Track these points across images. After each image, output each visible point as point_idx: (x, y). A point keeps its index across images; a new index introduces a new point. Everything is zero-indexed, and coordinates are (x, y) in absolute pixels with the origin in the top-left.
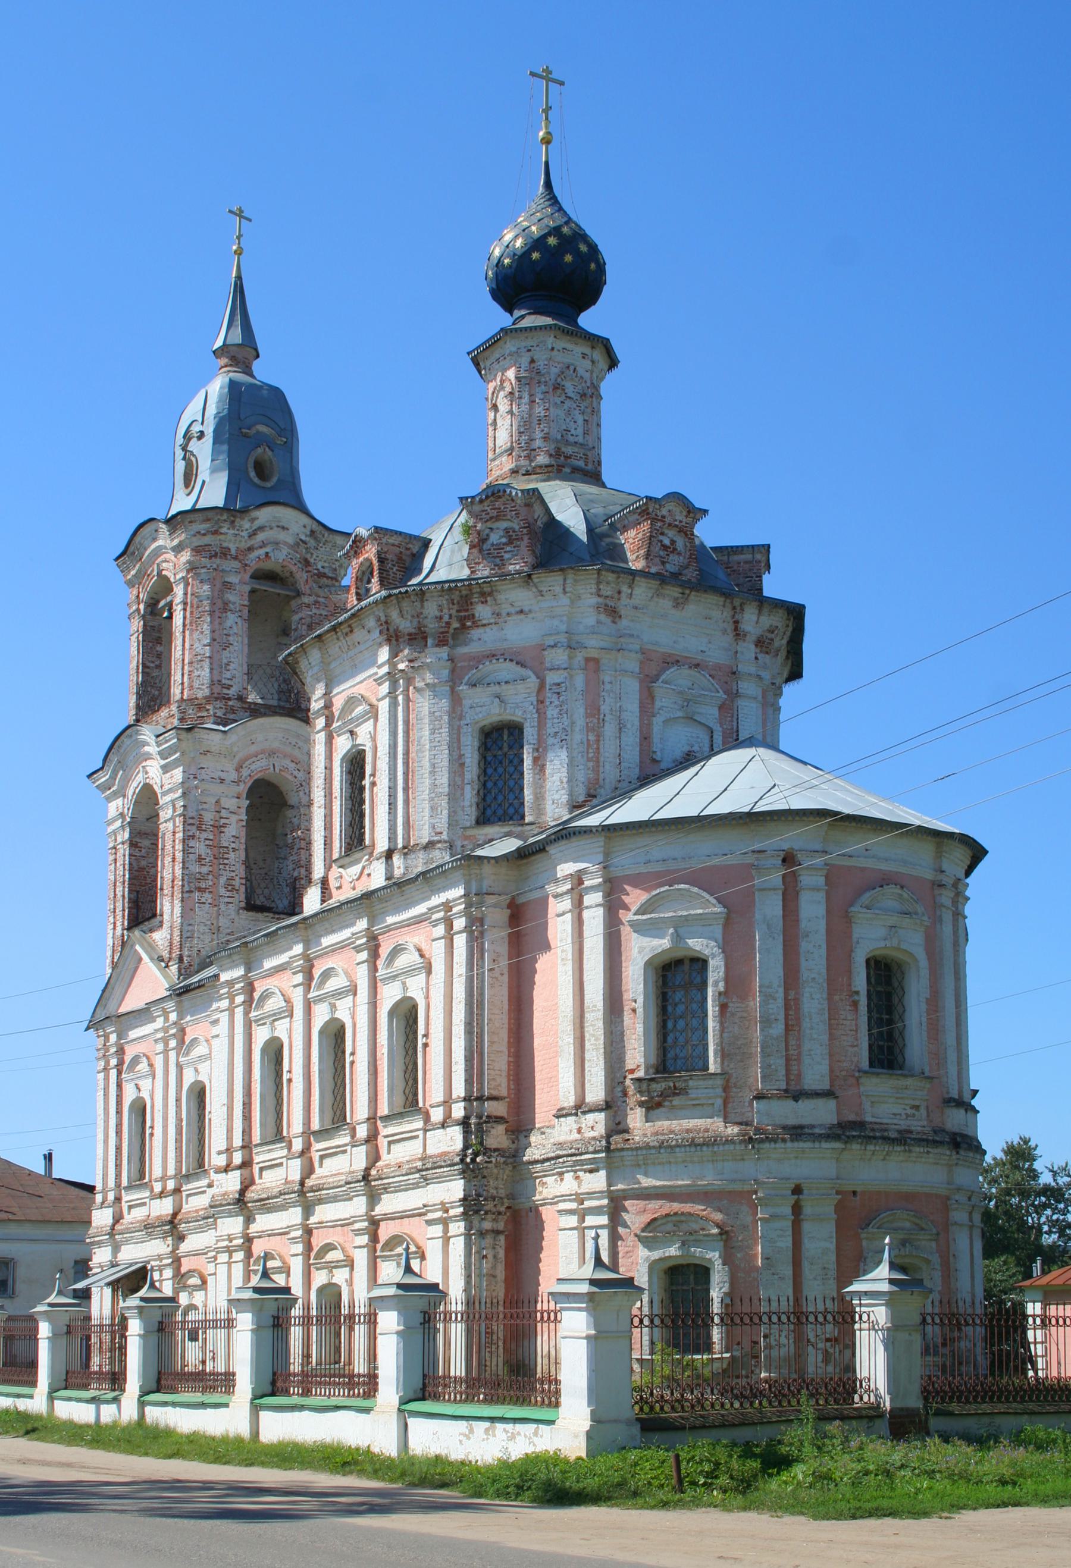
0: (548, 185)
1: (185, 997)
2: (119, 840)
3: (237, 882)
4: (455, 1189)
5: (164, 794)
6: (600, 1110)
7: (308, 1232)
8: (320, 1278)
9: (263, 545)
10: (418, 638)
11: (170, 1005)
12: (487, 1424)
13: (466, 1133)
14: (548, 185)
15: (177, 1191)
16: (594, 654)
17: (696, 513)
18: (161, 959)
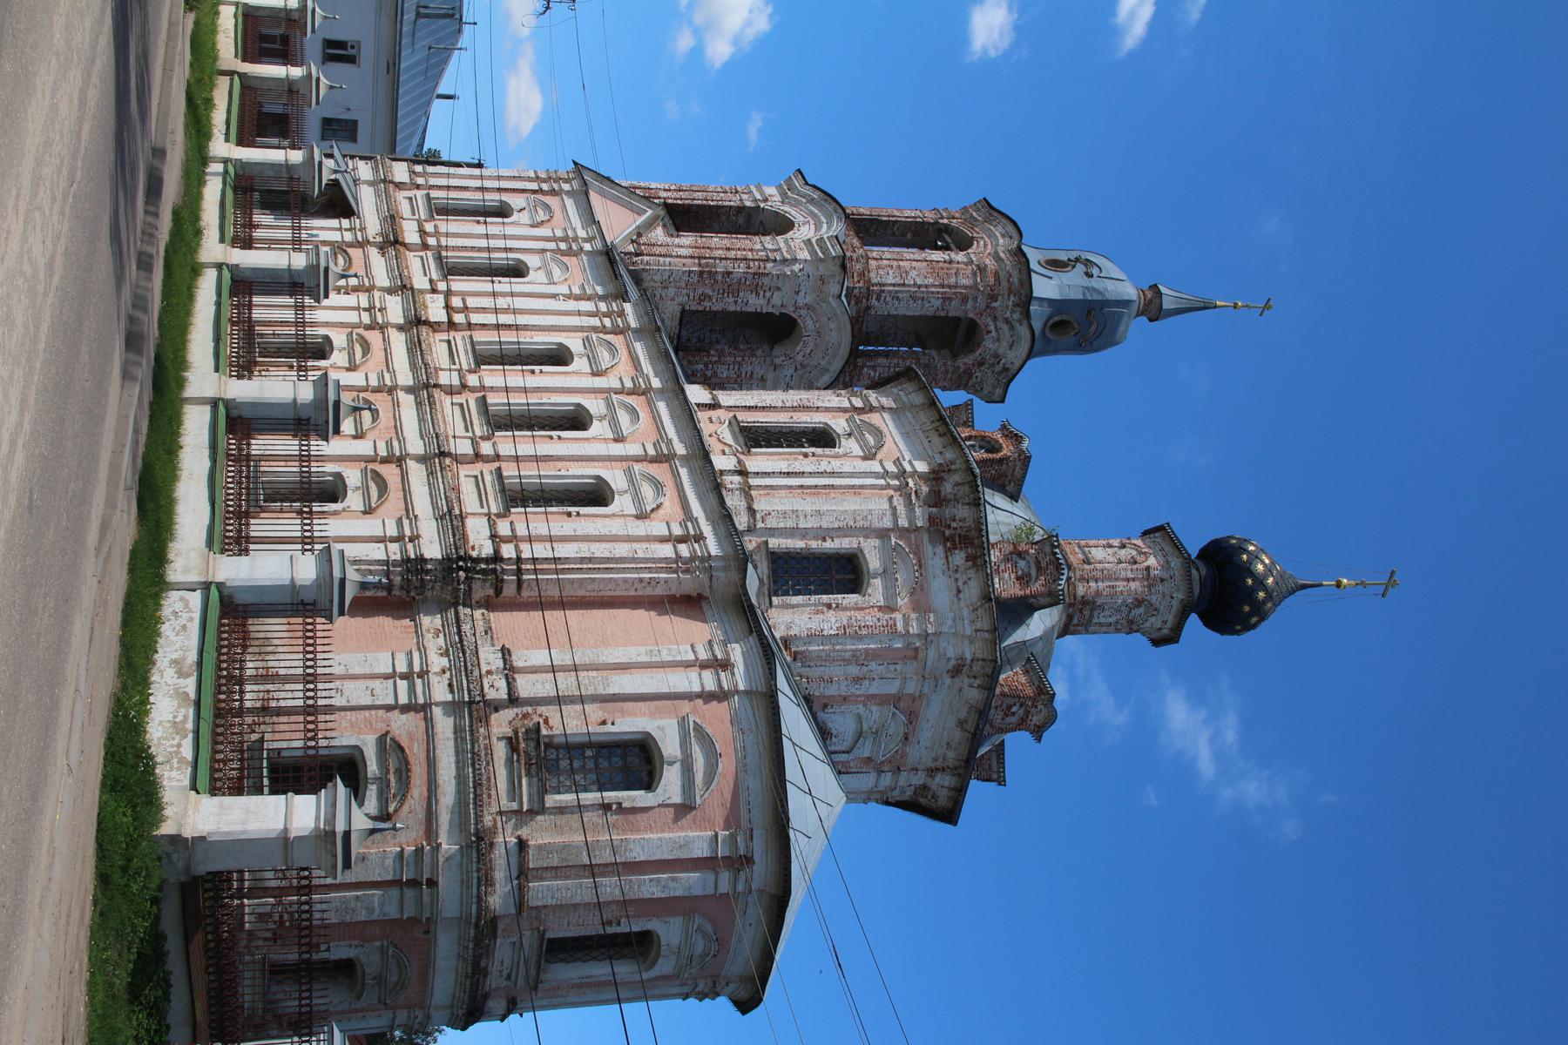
0: (1304, 587)
1: (605, 258)
2: (744, 197)
3: (707, 304)
4: (432, 550)
5: (786, 241)
6: (509, 694)
7: (391, 390)
8: (353, 476)
9: (997, 330)
10: (936, 499)
11: (599, 245)
12: (193, 695)
13: (487, 560)
14: (1304, 587)
15: (425, 246)
16: (921, 655)
17: (1038, 733)
18: (639, 235)
